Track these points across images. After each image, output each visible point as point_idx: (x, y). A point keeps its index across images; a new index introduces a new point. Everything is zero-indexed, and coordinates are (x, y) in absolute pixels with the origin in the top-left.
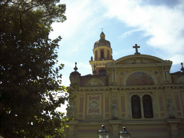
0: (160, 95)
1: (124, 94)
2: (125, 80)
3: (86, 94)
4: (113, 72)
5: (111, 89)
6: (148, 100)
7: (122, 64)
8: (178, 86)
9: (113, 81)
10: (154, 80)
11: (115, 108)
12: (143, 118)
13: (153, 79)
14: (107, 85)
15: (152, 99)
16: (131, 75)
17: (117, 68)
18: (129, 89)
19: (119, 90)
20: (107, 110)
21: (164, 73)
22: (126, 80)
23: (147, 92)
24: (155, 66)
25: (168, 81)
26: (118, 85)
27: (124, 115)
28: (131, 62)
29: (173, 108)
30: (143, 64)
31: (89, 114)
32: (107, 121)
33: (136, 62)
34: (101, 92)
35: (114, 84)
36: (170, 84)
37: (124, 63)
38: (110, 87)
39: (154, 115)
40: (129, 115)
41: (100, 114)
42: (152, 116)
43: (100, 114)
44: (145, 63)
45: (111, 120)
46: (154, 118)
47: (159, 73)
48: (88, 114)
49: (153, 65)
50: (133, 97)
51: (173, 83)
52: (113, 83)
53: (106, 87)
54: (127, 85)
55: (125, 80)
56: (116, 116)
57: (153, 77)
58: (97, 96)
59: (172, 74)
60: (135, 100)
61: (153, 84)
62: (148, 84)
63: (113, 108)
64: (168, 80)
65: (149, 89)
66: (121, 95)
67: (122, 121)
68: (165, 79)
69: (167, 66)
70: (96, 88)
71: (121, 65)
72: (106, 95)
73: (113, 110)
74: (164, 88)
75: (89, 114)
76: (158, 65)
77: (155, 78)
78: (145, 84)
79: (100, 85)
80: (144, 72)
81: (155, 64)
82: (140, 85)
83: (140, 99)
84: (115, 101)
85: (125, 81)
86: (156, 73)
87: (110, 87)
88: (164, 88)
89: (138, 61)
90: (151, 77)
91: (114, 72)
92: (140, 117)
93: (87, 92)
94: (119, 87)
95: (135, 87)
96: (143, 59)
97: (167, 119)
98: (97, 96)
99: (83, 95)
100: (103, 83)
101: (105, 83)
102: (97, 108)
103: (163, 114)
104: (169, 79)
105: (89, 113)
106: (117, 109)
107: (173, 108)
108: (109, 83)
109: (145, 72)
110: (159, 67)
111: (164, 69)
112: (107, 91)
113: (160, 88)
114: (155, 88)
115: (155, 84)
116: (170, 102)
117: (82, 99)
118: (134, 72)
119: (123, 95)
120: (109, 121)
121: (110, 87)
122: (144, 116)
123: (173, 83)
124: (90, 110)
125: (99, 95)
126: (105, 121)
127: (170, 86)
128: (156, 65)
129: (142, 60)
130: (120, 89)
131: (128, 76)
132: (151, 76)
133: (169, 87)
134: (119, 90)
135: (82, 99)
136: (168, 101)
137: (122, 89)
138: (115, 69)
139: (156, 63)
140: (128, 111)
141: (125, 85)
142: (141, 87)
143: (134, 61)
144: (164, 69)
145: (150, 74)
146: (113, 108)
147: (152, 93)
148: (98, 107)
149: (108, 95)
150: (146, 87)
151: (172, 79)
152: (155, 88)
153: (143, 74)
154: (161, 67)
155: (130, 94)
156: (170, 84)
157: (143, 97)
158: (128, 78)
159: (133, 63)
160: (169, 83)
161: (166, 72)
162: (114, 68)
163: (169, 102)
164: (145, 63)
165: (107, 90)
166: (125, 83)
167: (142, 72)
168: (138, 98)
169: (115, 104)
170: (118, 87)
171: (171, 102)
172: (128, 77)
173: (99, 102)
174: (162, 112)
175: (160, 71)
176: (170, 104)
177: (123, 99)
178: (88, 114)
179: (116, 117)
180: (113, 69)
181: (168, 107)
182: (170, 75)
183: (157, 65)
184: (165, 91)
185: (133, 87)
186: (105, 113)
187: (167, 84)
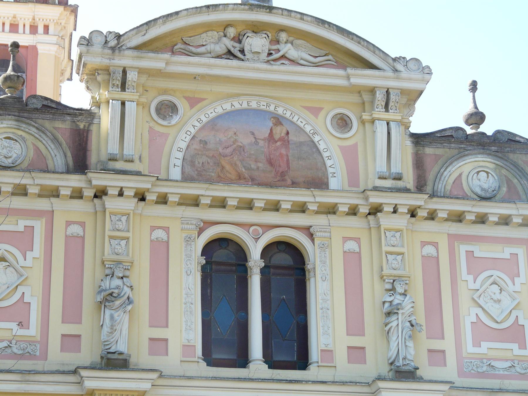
0: (351, 245)
1: (166, 229)
2: (180, 150)
3: (453, 238)
4: (379, 113)
5: (100, 194)
6: (289, 266)
7: (173, 53)
8: (444, 207)
9: (113, 148)
10: (329, 163)
11: (118, 303)
12: (258, 366)
13: (325, 155)
14: (80, 164)
15: (309, 267)
16: (212, 125)
17: (141, 71)
18: (195, 202)
19: (143, 199)
20: (72, 314)
21: (381, 129)
22: (184, 145)
23: (286, 227)
24: (342, 82)
25: (398, 178)
26: (138, 173)
27: (159, 345)
28: (220, 49)
29: (412, 325)
30: (276, 67)
31: (477, 350)
32: (75, 372)
33: (242, 51)
34: (43, 204)
35: (119, 165)
36: (406, 190)
37: (180, 46)
38: (100, 180)
39: (314, 354)
40: (187, 348)
41: (33, 330)
42: (302, 361)
43: (33, 330)
44: (293, 61)
45: (92, 367)
46: (313, 368)
47: (355, 123)
48: (470, 348)
49: (334, 76)
50: (209, 249)
51: (420, 188)
52: (113, 159)
53: (75, 181)
54: (186, 178)
55: (180, 150)
56: (122, 347)
57: (322, 146)
58: (21, 224)
59: (419, 139)
60: (223, 262)
61: (319, 183)
62: (294, 184)
63: (108, 299)
64: (395, 169)
65: (302, 208)
66: (153, 228)
67: (154, 375)
68: (381, 166)
69: (403, 92)
70: (17, 181)
71: (167, 56)
72: (69, 223)
73: (108, 312)
74: (375, 210)
75: (477, 350)
76: (362, 78)
77: (331, 146)
78: (281, 179)
79: (39, 166)
80: (280, 111)
81: (341, 72)
82: (255, 182)
83: (250, 264)
84: (119, 262)
85: (180, 155)
86: (343, 123)
87: (100, 180)
88: (375, 210)
89: (257, 43)
90: (314, 145)
91: (124, 96)
92: (242, 360)
93: (455, 228)
94: (149, 186)
95: (234, 193)
96: (283, 36)
97: (380, 378)
98: (21, 224)
99: (166, 229)
100: (58, 158)
101: (69, 154)
102: (16, 297)
103: (356, 353)
104: (403, 161)
105: (477, 344)
106: (129, 307)
107: (412, 325)
108: (93, 159)
109: (288, 115)
110: (359, 91)
111: (387, 107)
112: (77, 203)
113: (353, 211)
114: (331, 210)
115: (333, 183)
116: (400, 289)
117: (431, 264)
118: (227, 107)
119: (160, 234)
120: (84, 373)
121: (94, 182)
122: (264, 356)
123: (420, 188)
124: (477, 324)
125: (29, 223)
126: (63, 373)
127: (407, 201)
128: (348, 77)
129: (278, 42)
130: (150, 197)
131: (198, 125)
132: (316, 139)
133: (400, 210)
134: (143, 199)
135: (431, 264)
136: (389, 286)
137: (163, 200)
138: (132, 76)
139: (350, 71)
140: (186, 325)
141: (176, 173)
142: (261, 195)
143: (233, 39)
144: (387, 107)
145: (308, 129)
146: (108, 299)
147: (311, 236)
148: (21, 290)
149: (82, 224)
150: (287, 197)
151: (419, 164)
152: (331, 210)
153: (278, 120)
154: (372, 91)
155: (201, 231)
156: (406, 190)
157: (268, 251)
158: (194, 138)
159: (230, 54)
160: (400, 184)
161: (392, 124)
162: (124, 72)
163: (393, 289)
164: (293, 61)
165: (77, 195)
166: (179, 163)
167: (272, 108)
168: (241, 254)
169: (117, 282)
170: (143, 184)
171: (404, 294)
172: (193, 131)
173: (29, 263)
174: (356, 341)
175: (366, 116)
176: (398, 299)
177: (161, 251)
178: (470, 348)
179: (121, 353)
180: (119, 76)
181: (389, 314)
182: (409, 143)
183: (353, 80)
184: (379, 227)
185: (220, 191)
186: (58, 329)
187: (391, 190)
